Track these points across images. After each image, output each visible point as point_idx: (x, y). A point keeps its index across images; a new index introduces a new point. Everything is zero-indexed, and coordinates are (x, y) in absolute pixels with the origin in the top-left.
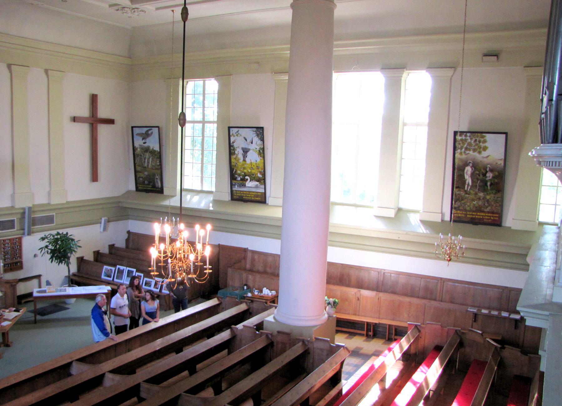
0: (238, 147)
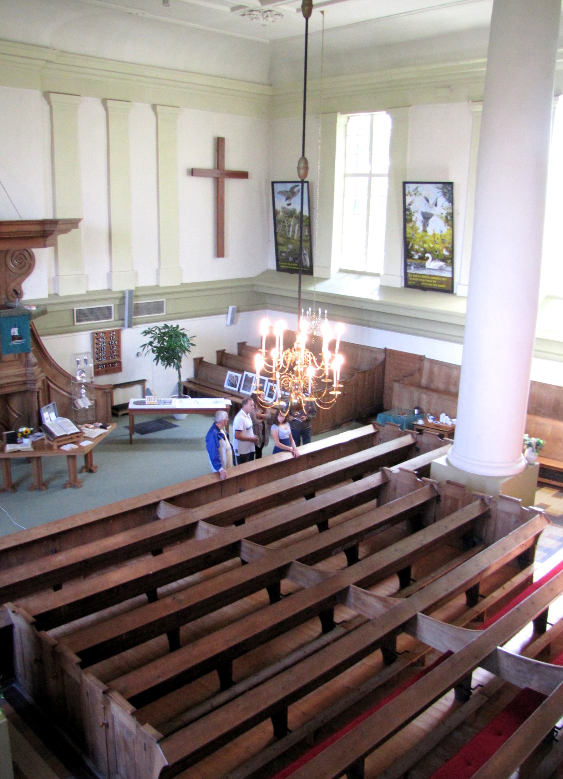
0: (417, 211)
